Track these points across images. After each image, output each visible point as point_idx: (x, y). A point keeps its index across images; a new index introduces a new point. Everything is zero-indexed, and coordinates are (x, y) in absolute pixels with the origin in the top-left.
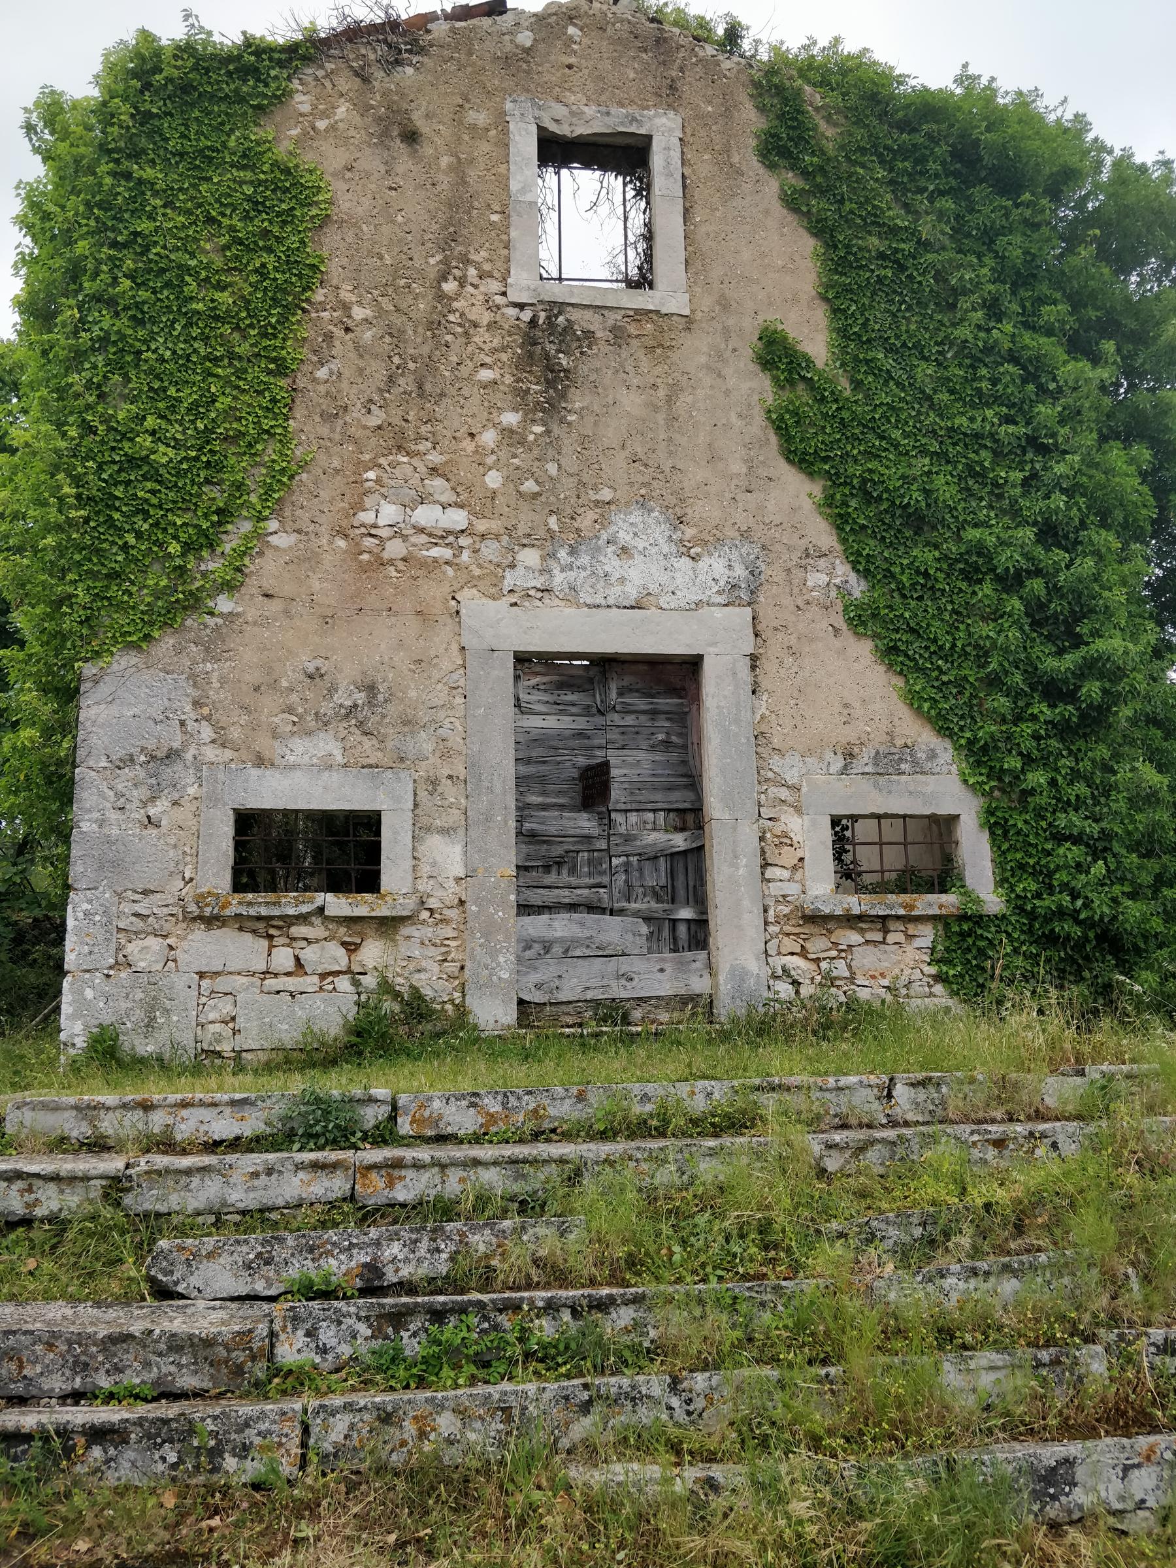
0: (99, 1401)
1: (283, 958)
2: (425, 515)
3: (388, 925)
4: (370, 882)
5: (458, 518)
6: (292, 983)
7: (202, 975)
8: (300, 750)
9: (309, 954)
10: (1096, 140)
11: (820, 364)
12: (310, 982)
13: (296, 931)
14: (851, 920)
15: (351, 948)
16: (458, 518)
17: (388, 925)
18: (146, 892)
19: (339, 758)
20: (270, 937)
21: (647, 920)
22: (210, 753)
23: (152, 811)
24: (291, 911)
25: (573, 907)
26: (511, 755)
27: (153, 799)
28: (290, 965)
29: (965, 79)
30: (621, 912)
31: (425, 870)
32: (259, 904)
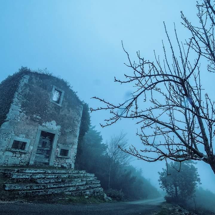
0: (40, 146)
1: (14, 155)
2: (38, 117)
3: (25, 153)
4: (24, 149)
5: (40, 118)
6: (14, 158)
7: (6, 156)
8: (21, 135)
9: (17, 155)
10: (195, 195)
11: (47, 124)
12: (16, 158)
13: (16, 153)
14: (60, 158)
15: (21, 155)
16: (40, 118)
17: (25, 153)
18: (3, 147)
19: (25, 137)
20: (14, 153)
21: (45, 156)
22: (13, 134)
23: (6, 139)
24: (17, 151)
25: (39, 154)
26: (39, 139)
27: (6, 138)
28: (15, 156)
29: (62, 79)
30: (43, 154)
31: (29, 149)
32: (14, 150)
